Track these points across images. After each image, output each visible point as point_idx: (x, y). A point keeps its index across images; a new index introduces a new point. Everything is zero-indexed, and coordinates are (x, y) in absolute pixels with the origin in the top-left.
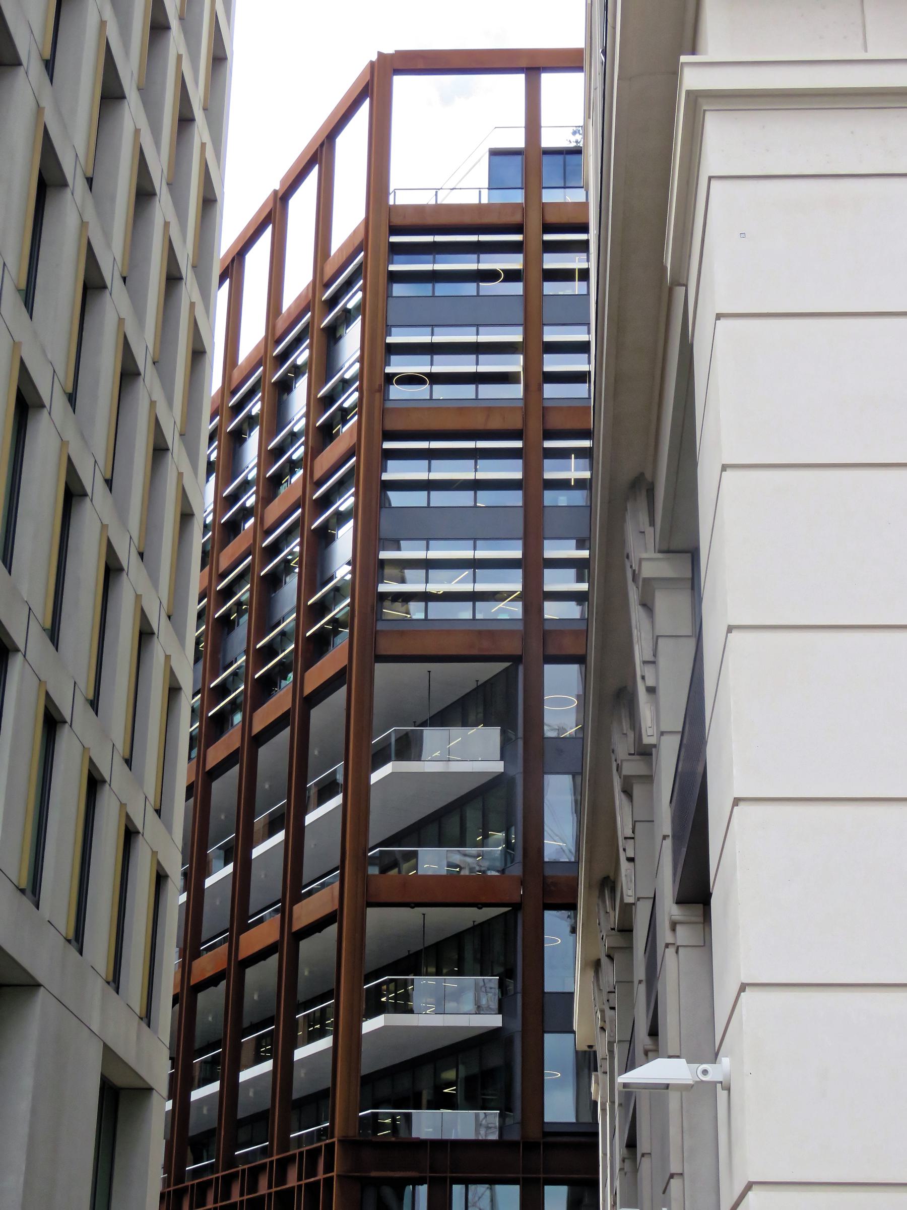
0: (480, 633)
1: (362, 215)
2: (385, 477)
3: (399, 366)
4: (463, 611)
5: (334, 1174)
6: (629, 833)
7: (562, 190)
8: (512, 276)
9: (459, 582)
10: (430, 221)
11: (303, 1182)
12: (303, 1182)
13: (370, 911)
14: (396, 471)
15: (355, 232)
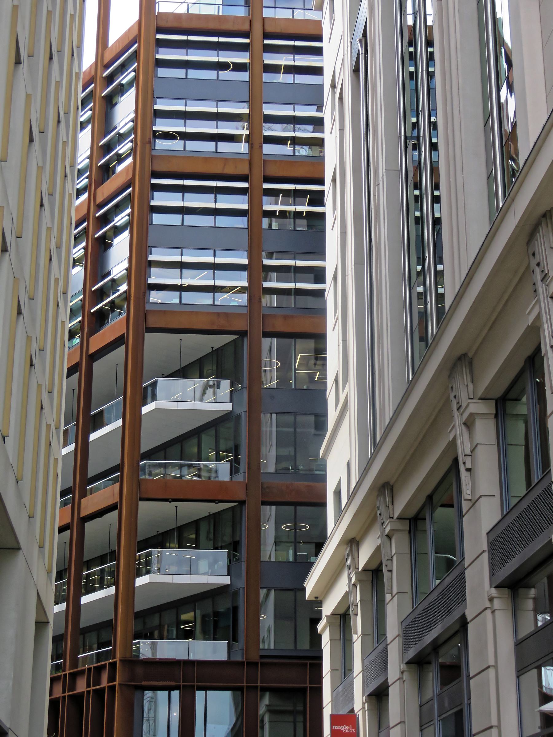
0: (218, 314)
1: (137, 18)
2: (153, 203)
3: (163, 126)
4: (206, 299)
5: (116, 683)
6: (468, 452)
7: (273, 9)
8: (239, 67)
9: (199, 279)
10: (185, 25)
11: (91, 689)
12: (91, 689)
13: (141, 504)
14: (160, 199)
15: (129, 29)
